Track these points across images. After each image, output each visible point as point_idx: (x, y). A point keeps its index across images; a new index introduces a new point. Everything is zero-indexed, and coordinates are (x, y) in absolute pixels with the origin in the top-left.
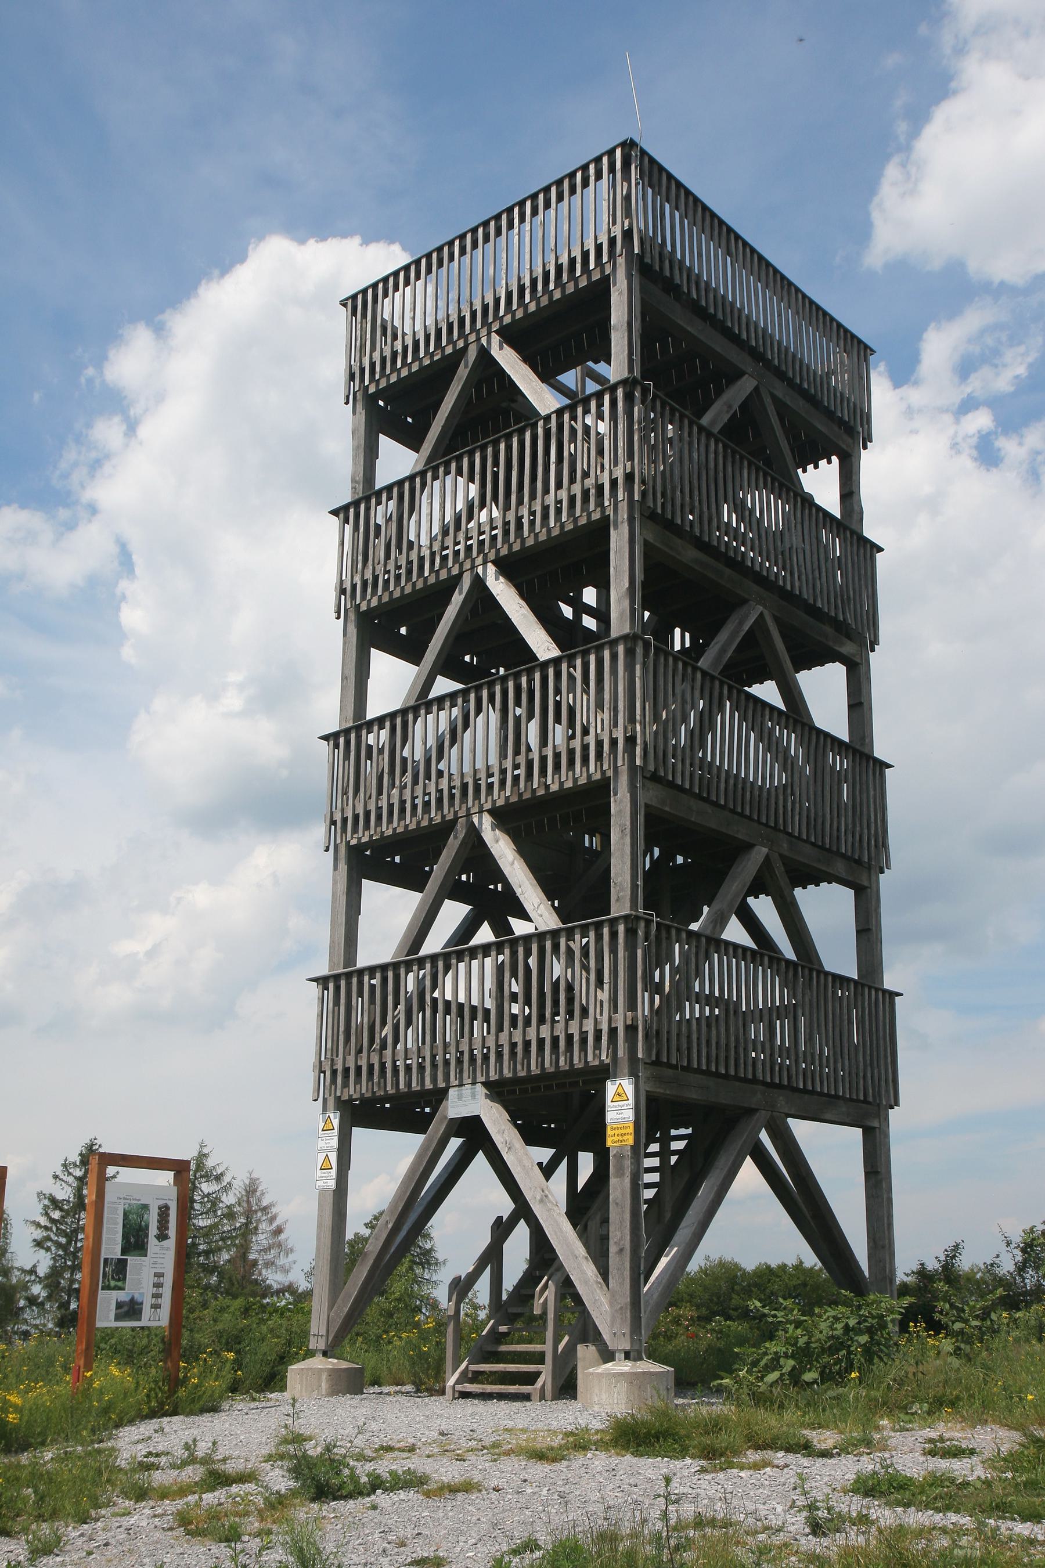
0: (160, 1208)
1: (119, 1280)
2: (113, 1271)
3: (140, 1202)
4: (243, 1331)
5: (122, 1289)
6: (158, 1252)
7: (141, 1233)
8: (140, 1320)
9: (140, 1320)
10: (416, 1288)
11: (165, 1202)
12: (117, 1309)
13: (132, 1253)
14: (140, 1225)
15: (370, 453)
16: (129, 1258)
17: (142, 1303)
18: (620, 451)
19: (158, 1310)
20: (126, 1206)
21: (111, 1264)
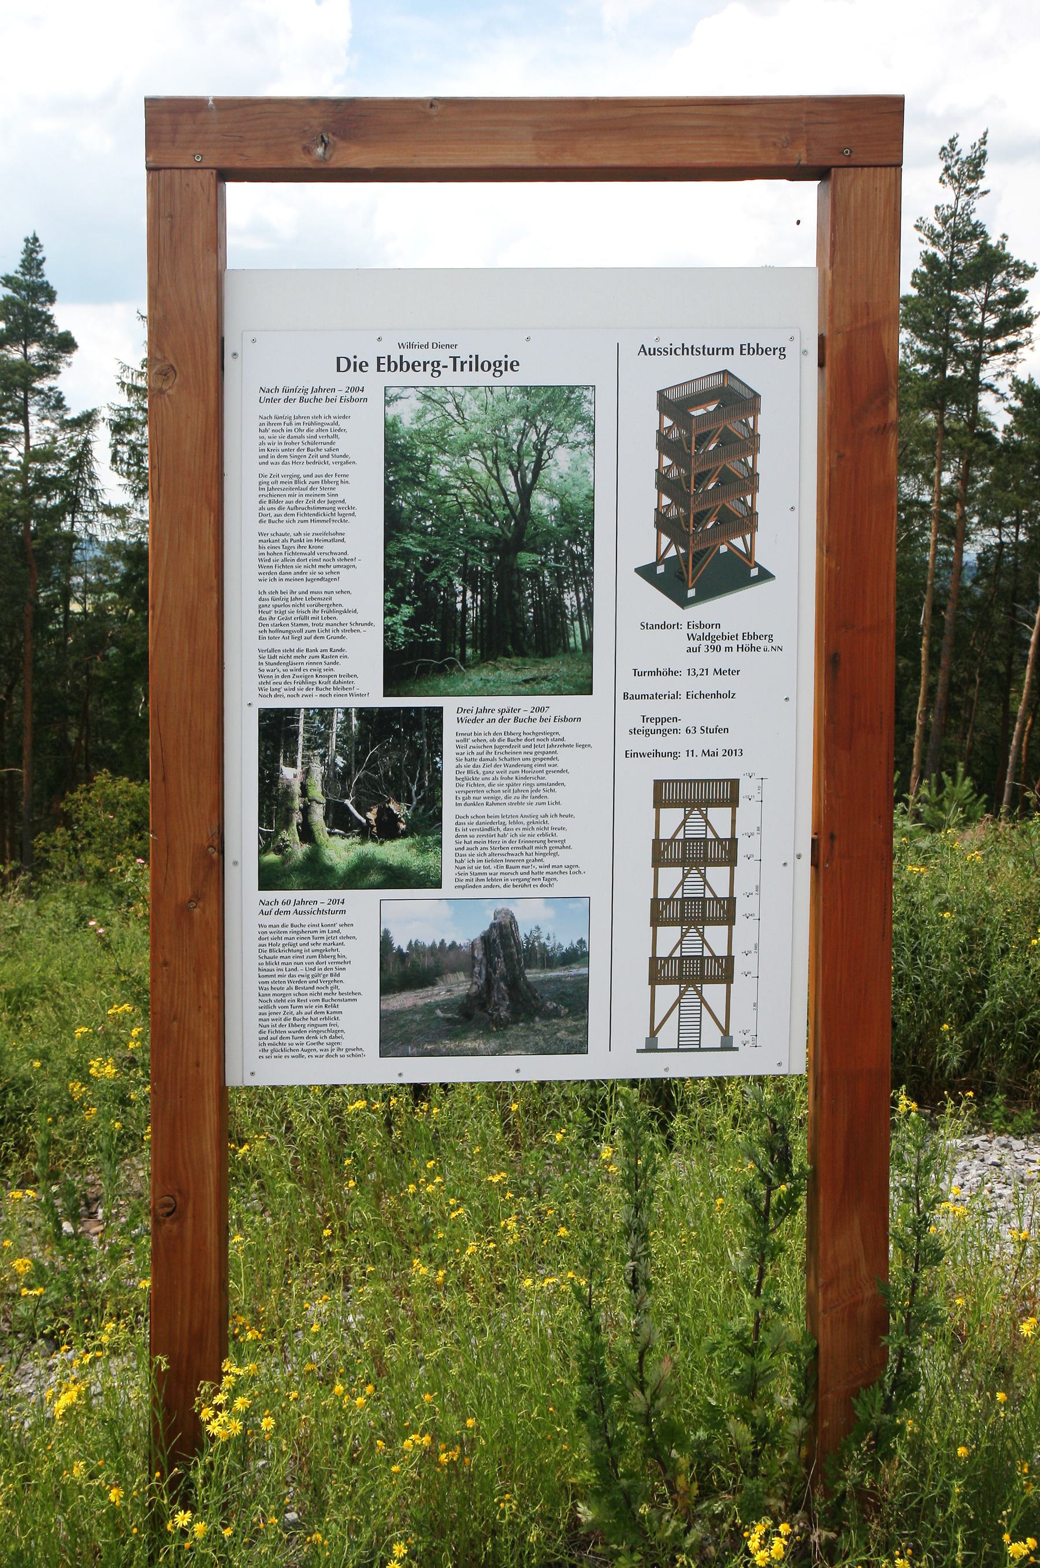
0: (666, 404)
1: (387, 829)
2: (334, 780)
3: (509, 378)
4: (357, 1115)
5: (430, 880)
6: (682, 661)
7: (526, 559)
8: (580, 1047)
9: (580, 1047)
10: (563, 1131)
11: (719, 363)
12: (387, 988)
13: (475, 676)
14: (523, 514)
15: (898, 661)
16: (449, 705)
17: (578, 955)
18: (820, 1047)
19: (714, 993)
20: (406, 412)
21: (317, 741)
